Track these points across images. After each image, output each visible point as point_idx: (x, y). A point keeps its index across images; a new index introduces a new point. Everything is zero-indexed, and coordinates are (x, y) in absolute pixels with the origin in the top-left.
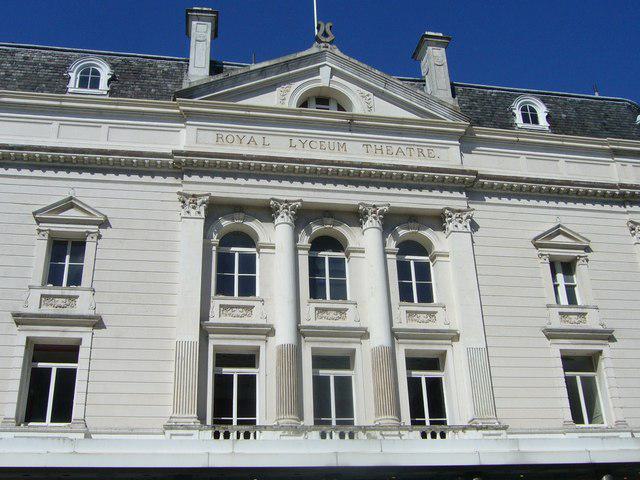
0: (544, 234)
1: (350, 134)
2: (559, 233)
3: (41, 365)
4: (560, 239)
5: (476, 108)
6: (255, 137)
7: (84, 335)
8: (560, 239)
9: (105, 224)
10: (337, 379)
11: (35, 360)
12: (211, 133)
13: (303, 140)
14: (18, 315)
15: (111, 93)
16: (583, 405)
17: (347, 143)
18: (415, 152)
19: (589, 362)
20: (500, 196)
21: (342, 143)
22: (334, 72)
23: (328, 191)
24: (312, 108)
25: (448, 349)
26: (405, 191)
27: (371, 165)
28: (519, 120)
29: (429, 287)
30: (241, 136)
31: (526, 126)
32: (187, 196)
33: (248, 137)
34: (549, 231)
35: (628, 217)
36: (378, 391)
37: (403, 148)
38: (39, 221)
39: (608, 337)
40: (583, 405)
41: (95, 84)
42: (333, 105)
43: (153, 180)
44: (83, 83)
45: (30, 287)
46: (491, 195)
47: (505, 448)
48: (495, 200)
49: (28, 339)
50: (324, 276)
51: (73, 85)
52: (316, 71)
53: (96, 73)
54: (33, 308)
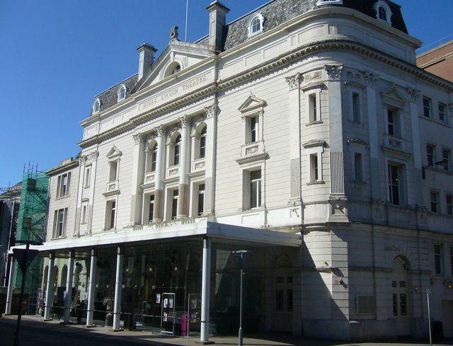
0: (243, 105)
2: (252, 100)
3: (253, 181)
4: (253, 104)
7: (261, 164)
8: (253, 104)
9: (265, 104)
11: (251, 179)
14: (240, 160)
16: (252, 199)
19: (255, 174)
20: (231, 89)
22: (175, 53)
25: (263, 165)
26: (194, 104)
27: (189, 94)
32: (290, 78)
34: (246, 101)
35: (131, 135)
38: (242, 112)
39: (266, 157)
40: (252, 199)
43: (289, 68)
45: (242, 146)
46: (227, 90)
47: (124, 236)
48: (229, 92)
49: (244, 171)
52: (169, 57)
54: (244, 156)
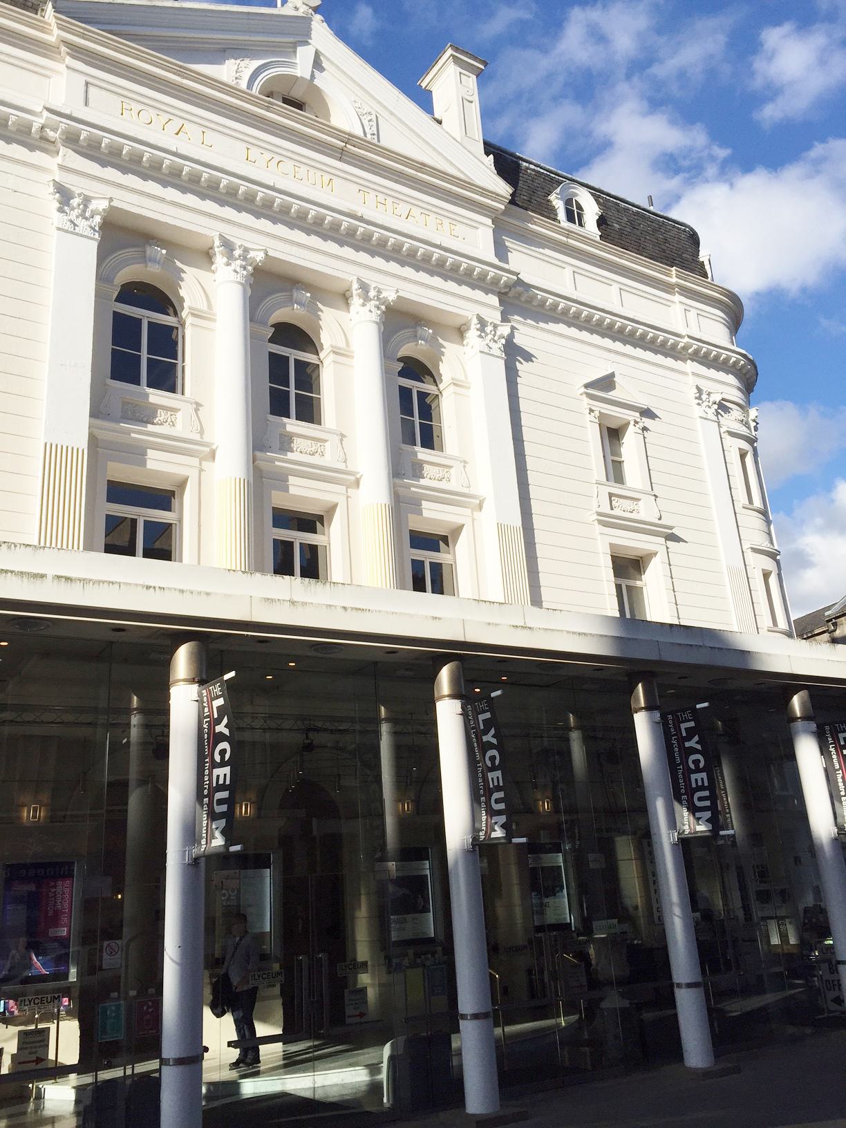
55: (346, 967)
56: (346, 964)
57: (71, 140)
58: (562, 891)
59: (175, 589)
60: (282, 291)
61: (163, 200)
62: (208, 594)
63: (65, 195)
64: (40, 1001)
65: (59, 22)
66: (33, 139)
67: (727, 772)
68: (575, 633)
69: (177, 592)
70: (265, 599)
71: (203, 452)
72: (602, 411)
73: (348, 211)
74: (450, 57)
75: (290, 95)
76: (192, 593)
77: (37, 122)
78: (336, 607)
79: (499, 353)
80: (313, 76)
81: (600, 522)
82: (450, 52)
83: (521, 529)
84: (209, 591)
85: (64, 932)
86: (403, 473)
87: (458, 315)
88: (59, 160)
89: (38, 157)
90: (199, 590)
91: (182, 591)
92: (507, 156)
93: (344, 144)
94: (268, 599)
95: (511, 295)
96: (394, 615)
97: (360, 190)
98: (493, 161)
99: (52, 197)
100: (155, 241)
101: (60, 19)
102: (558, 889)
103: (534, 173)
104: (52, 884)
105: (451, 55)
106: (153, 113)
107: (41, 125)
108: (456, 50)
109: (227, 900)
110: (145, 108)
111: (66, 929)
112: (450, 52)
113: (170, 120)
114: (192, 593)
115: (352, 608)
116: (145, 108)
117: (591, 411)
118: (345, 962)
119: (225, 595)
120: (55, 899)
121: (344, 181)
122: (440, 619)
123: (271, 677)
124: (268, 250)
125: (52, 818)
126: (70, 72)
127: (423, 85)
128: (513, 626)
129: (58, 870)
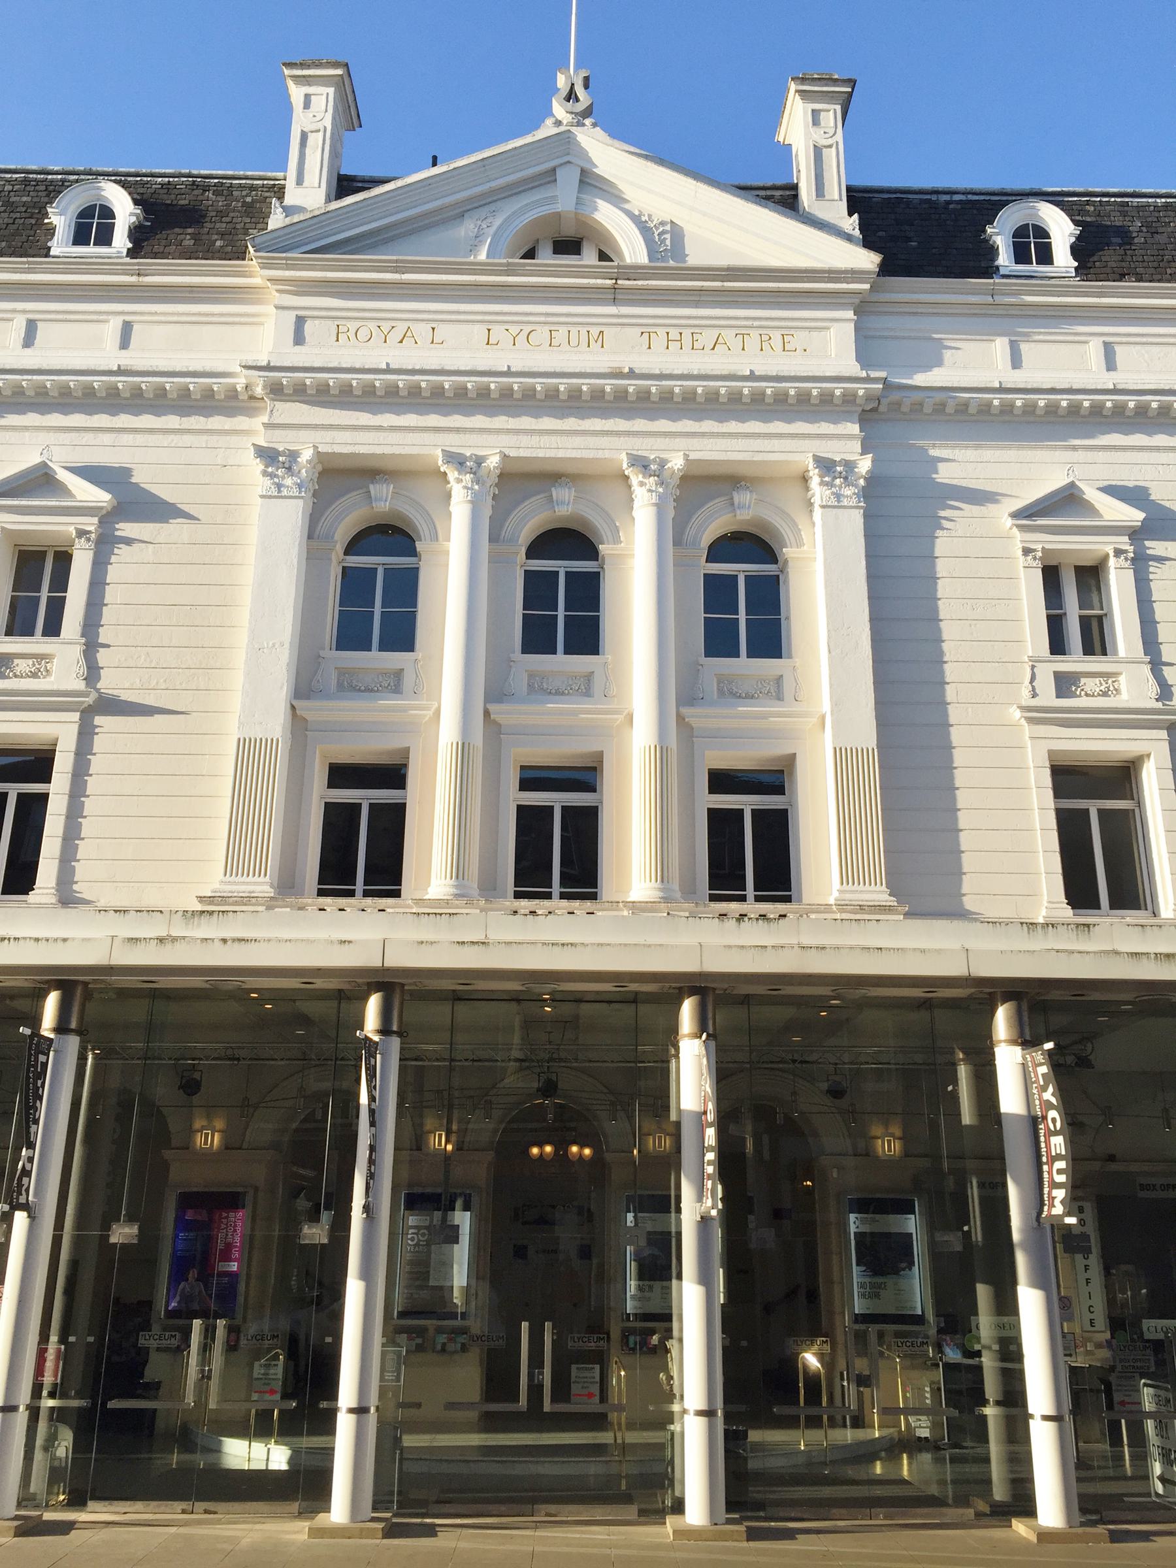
1: (612, 310)
5: (910, 239)
6: (415, 327)
10: (21, 796)
12: (477, 327)
13: (514, 330)
15: (132, 253)
17: (606, 330)
18: (659, 341)
21: (595, 331)
23: (1157, 449)
24: (546, 258)
28: (1005, 259)
29: (346, 597)
30: (386, 326)
31: (1022, 268)
33: (401, 327)
36: (1157, 897)
37: (728, 334)
41: (105, 237)
42: (589, 257)
44: (81, 237)
50: (373, 605)
51: (60, 245)
53: (107, 213)
55: (902, 1344)
56: (150, 1333)
57: (276, 391)
58: (910, 1269)
59: (30, 938)
60: (538, 493)
61: (379, 428)
62: (65, 940)
63: (268, 455)
64: (158, 1337)
65: (260, 261)
66: (243, 401)
67: (967, 1117)
68: (557, 944)
69: (32, 941)
70: (128, 939)
71: (425, 716)
72: (1048, 546)
73: (609, 370)
74: (795, 95)
75: (563, 234)
76: (48, 940)
77: (240, 383)
78: (213, 940)
79: (853, 502)
80: (579, 202)
81: (1030, 720)
82: (793, 87)
83: (876, 750)
84: (65, 937)
85: (234, 1267)
86: (701, 696)
87: (787, 462)
88: (265, 418)
89: (241, 422)
90: (56, 937)
91: (37, 940)
92: (910, 196)
93: (614, 281)
94: (132, 939)
95: (882, 408)
96: (288, 942)
97: (642, 333)
98: (857, 221)
99: (255, 462)
100: (381, 475)
101: (261, 258)
102: (903, 1265)
103: (959, 206)
104: (225, 1215)
105: (797, 91)
106: (372, 325)
107: (244, 385)
108: (803, 80)
109: (415, 1245)
110: (363, 324)
111: (236, 1264)
112: (793, 87)
113: (393, 327)
114: (47, 940)
115: (234, 940)
116: (363, 324)
117: (1027, 551)
118: (150, 1331)
119: (84, 940)
120: (227, 1231)
121: (618, 329)
122: (350, 942)
123: (270, 1006)
124: (503, 450)
125: (227, 1146)
126: (280, 311)
127: (781, 140)
128: (458, 942)
129: (231, 1201)
